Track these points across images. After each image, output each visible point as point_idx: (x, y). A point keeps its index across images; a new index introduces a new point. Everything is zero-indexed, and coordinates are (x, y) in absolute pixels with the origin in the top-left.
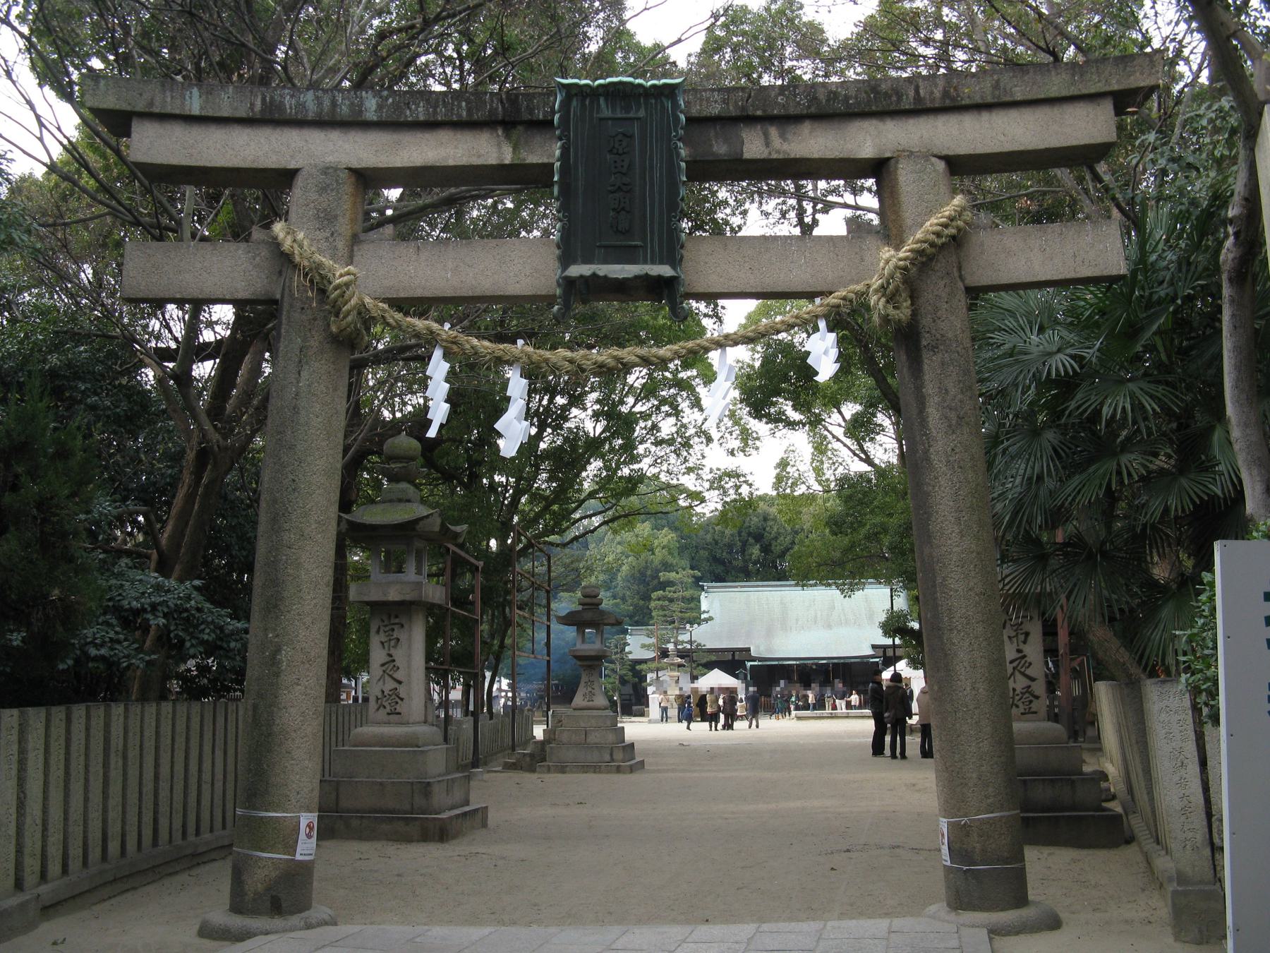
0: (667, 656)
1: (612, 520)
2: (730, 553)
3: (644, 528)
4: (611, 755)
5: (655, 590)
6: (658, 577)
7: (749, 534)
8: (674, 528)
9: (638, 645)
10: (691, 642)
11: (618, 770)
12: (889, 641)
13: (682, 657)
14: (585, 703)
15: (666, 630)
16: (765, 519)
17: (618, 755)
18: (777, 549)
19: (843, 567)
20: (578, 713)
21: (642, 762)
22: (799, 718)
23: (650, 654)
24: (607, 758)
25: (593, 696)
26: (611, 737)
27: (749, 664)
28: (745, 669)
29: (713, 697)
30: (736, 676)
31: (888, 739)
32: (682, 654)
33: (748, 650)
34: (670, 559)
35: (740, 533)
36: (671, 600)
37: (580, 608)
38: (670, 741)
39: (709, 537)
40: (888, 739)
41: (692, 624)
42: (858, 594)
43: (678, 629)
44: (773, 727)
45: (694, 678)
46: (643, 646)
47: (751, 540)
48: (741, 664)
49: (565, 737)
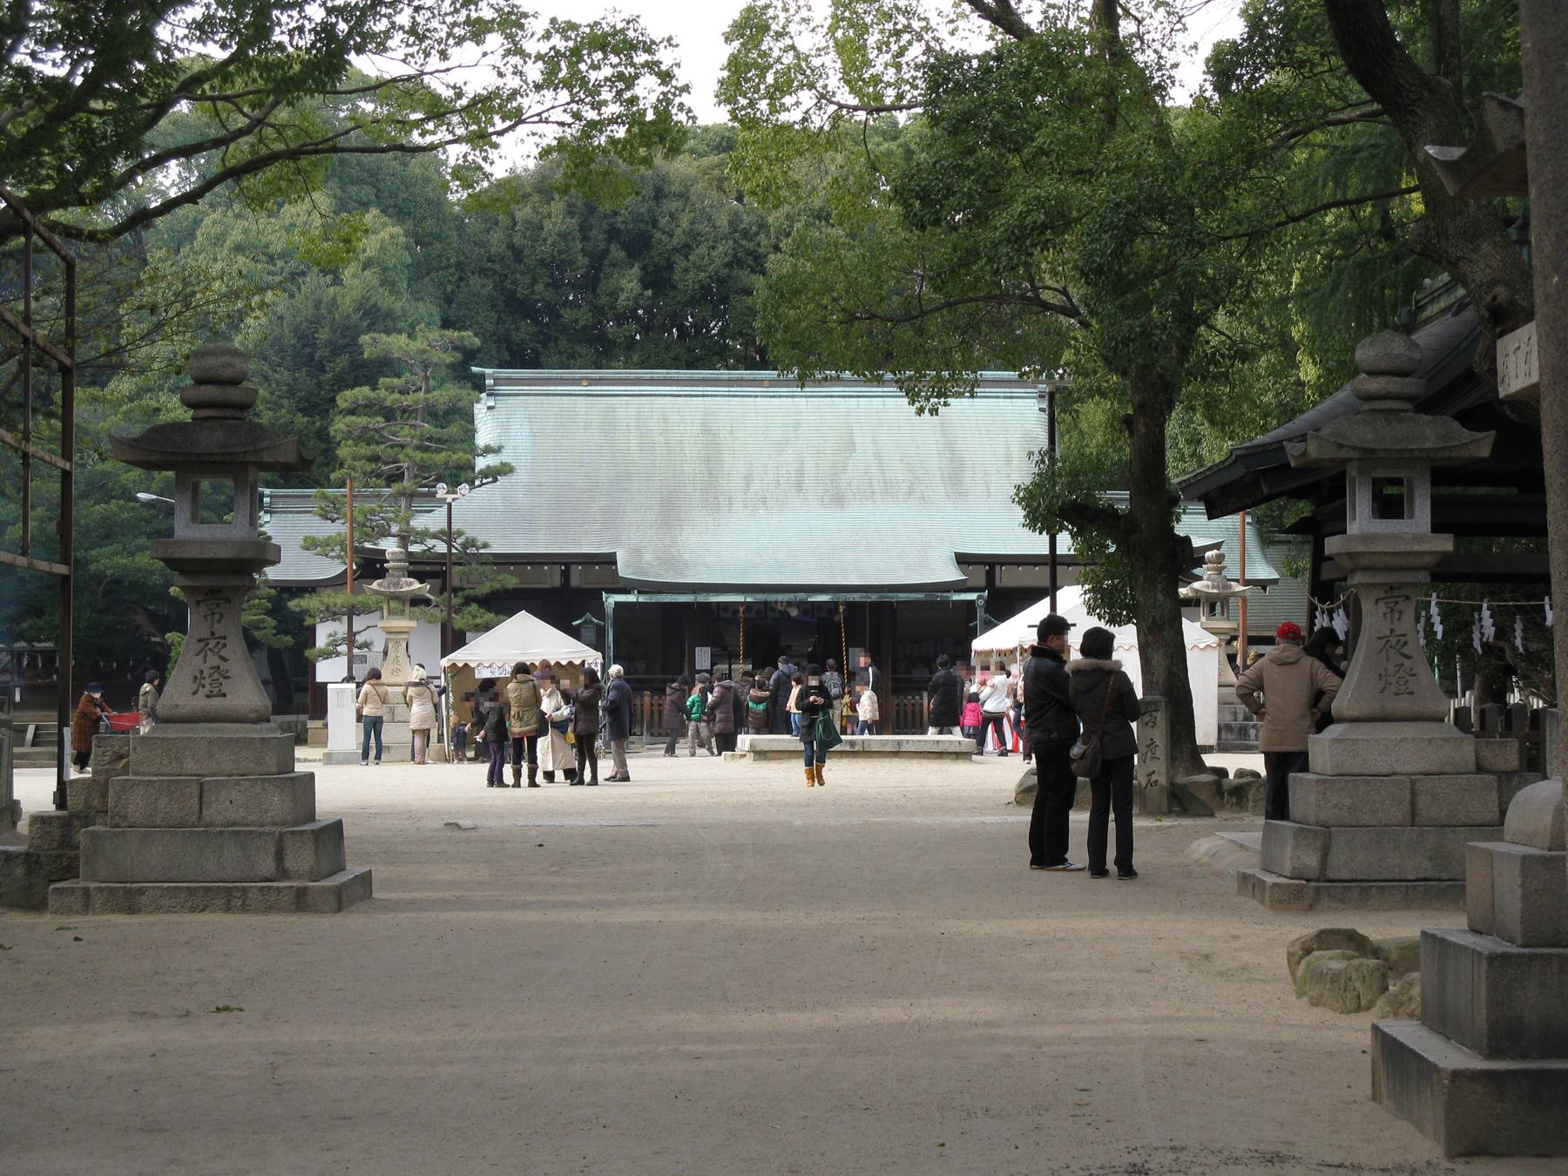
0: (381, 573)
1: (255, 165)
2: (556, 285)
3: (306, 214)
4: (279, 856)
5: (344, 383)
6: (352, 346)
7: (613, 234)
8: (399, 211)
9: (299, 539)
10: (448, 535)
11: (301, 902)
12: (1037, 544)
13: (421, 577)
14: (199, 703)
15: (378, 501)
16: (659, 194)
17: (301, 858)
18: (688, 278)
19: (909, 337)
20: (174, 732)
21: (366, 879)
22: (760, 754)
23: (330, 568)
24: (267, 865)
25: (199, 678)
26: (278, 804)
27: (611, 600)
28: (600, 611)
29: (526, 692)
30: (575, 633)
31: (1079, 819)
32: (422, 568)
33: (609, 560)
34: (385, 299)
35: (584, 229)
36: (389, 414)
37: (186, 415)
38: (410, 815)
39: (496, 240)
40: (1079, 819)
41: (454, 484)
42: (959, 408)
43: (412, 496)
44: (674, 780)
45: (453, 640)
46: (311, 544)
47: (617, 253)
48: (589, 599)
49: (136, 805)
